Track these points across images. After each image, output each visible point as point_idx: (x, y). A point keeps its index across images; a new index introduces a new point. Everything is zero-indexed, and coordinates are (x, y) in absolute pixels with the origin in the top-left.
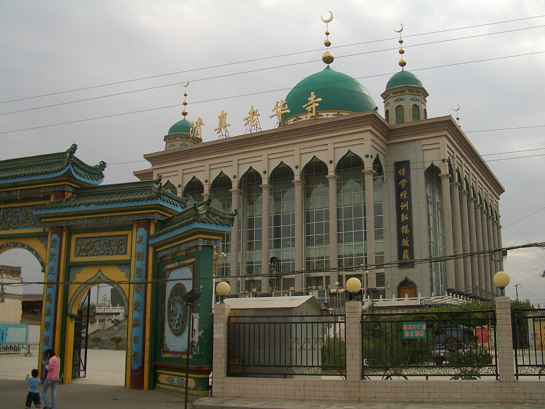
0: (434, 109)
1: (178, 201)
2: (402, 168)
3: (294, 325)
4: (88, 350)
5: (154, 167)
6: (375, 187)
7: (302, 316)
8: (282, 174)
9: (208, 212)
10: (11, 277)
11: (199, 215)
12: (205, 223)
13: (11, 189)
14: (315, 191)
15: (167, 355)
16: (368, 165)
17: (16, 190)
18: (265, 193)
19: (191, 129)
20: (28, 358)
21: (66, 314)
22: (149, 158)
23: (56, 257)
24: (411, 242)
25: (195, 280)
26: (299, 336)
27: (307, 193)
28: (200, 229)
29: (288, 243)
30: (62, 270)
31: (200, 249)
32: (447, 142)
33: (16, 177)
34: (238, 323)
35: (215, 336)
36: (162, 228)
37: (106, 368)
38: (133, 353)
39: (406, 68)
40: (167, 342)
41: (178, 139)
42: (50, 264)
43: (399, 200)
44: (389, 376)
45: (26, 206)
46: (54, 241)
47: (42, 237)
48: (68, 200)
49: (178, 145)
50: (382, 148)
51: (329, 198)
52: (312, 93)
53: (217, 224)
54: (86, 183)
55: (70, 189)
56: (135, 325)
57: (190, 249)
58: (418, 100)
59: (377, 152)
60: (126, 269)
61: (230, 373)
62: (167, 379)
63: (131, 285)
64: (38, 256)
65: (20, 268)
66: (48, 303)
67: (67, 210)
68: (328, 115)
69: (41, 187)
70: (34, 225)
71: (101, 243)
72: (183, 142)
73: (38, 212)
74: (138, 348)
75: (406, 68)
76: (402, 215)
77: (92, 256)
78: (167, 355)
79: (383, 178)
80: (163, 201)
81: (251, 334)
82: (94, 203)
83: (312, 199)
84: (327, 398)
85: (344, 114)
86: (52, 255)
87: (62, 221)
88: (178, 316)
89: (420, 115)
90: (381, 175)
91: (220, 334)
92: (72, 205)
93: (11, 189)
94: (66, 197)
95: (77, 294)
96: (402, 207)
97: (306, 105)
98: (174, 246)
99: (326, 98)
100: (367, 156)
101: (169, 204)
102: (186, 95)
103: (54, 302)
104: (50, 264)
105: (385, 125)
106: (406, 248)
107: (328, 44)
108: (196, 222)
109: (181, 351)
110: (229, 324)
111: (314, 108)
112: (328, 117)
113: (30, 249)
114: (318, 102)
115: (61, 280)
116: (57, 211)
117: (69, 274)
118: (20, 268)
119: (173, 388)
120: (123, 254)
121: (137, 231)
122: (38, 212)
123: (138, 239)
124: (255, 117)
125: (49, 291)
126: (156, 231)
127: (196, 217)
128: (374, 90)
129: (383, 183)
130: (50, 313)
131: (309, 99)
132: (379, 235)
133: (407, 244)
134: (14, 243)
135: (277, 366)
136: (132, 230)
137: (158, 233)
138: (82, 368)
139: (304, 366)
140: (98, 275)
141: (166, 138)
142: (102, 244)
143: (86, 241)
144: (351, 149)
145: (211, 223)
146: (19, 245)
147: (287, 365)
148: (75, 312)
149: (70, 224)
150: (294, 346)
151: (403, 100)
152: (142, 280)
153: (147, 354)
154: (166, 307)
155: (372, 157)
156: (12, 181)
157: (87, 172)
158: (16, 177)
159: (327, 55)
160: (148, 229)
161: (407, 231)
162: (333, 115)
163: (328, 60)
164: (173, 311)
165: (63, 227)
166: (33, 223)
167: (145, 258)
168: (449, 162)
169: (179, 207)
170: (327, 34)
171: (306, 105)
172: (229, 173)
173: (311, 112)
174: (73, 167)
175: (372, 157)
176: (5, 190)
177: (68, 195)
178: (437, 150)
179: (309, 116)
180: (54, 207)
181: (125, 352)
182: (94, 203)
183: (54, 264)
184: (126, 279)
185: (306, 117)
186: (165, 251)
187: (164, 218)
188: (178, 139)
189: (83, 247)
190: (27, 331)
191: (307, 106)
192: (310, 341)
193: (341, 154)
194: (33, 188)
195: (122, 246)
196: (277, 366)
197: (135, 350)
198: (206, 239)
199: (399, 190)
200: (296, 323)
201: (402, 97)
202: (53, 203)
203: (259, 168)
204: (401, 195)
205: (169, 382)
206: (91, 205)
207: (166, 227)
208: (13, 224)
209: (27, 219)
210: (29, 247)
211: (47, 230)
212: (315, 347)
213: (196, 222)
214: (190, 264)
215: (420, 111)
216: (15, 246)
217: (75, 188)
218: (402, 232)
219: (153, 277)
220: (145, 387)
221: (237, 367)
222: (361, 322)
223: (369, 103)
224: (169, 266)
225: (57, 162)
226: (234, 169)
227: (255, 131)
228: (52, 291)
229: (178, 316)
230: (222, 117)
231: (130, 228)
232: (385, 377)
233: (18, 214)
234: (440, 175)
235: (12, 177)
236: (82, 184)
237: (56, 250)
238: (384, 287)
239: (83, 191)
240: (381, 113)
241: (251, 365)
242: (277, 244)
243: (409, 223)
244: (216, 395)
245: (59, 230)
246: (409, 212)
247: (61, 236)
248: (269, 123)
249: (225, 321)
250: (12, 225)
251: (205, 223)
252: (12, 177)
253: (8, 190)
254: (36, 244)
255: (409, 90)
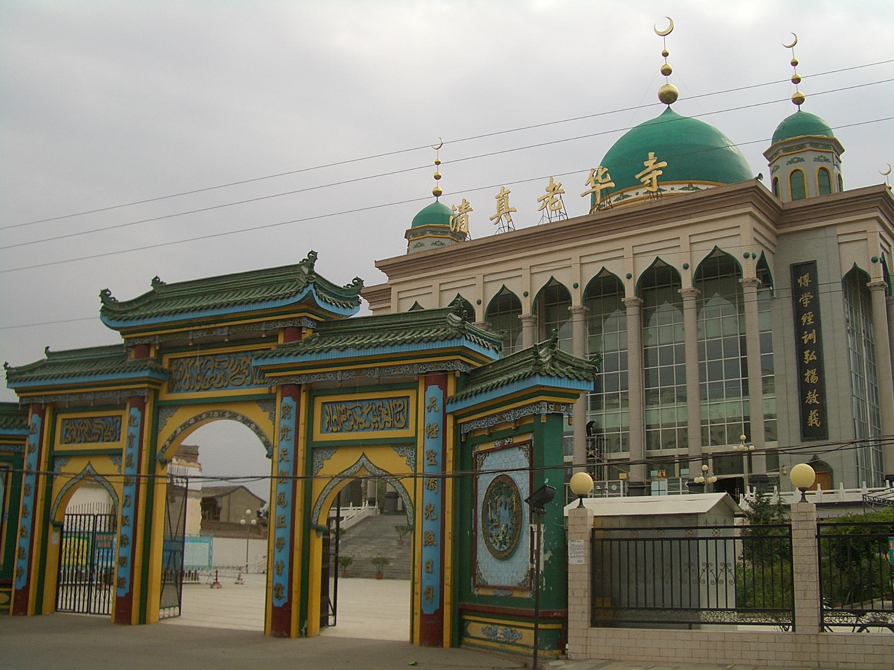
0: (855, 174)
1: (490, 341)
2: (804, 271)
3: (702, 543)
4: (339, 580)
5: (392, 282)
6: (761, 305)
7: (716, 527)
8: (604, 289)
9: (553, 359)
10: (184, 462)
11: (541, 365)
12: (551, 376)
13: (212, 326)
14: (655, 316)
15: (482, 592)
16: (749, 271)
17: (221, 327)
18: (577, 318)
19: (451, 218)
20: (215, 591)
21: (308, 526)
22: (385, 266)
23: (292, 434)
24: (822, 397)
25: (534, 470)
26: (712, 560)
27: (645, 318)
28: (544, 386)
29: (615, 401)
30: (301, 454)
31: (544, 420)
32: (879, 229)
33: (222, 306)
34: (608, 540)
35: (572, 561)
36: (466, 385)
37: (374, 610)
38: (424, 589)
39: (804, 108)
40: (482, 571)
41: (428, 234)
42: (281, 446)
43: (800, 328)
44: (863, 627)
45: (237, 353)
46: (286, 408)
47: (266, 401)
48: (308, 341)
49: (428, 245)
50: (767, 239)
51: (687, 327)
52: (651, 155)
53: (571, 379)
54: (333, 313)
55: (310, 324)
56: (427, 543)
57: (522, 419)
58: (827, 160)
59: (761, 248)
60: (409, 452)
61: (596, 622)
62: (483, 630)
64: (258, 432)
65: (197, 447)
66: (279, 508)
67: (307, 358)
68: (672, 189)
69: (262, 322)
70: (252, 383)
71: (364, 410)
72: (437, 240)
73: (260, 363)
74: (432, 581)
75: (804, 108)
76: (807, 353)
77: (350, 431)
78: (482, 592)
79: (772, 291)
80: (468, 342)
81: (639, 556)
82: (354, 346)
83: (651, 330)
84: (763, 663)
85: (703, 187)
86: (285, 430)
87: (300, 375)
88: (502, 529)
89: (832, 185)
90: (768, 286)
91: (579, 557)
92: (317, 350)
93: (212, 326)
94: (304, 337)
95: (325, 493)
96: (806, 338)
97: (641, 174)
98: (494, 415)
99: (667, 162)
100: (746, 256)
101: (477, 346)
103: (289, 507)
104: (281, 446)
105: (775, 204)
106: (813, 406)
107: (667, 72)
108: (538, 376)
109: (509, 585)
110: (593, 540)
111: (655, 178)
112: (673, 192)
113: (246, 421)
114: (660, 169)
115: (300, 473)
116: (292, 360)
117: (312, 461)
118: (197, 447)
119: (497, 645)
120: (402, 428)
121: (425, 391)
122: (260, 363)
123: (428, 404)
124: (557, 196)
125: (282, 488)
126: (457, 391)
127: (537, 368)
128: (750, 147)
129: (773, 299)
130: (284, 524)
131: (646, 164)
132: (768, 385)
133: (815, 401)
134: (218, 411)
135: (677, 609)
136: (417, 388)
137: (459, 394)
138: (331, 612)
139: (722, 610)
140: (361, 463)
141: (408, 234)
142: (366, 412)
143: (338, 407)
144: (721, 245)
145: (560, 377)
146: (227, 415)
147: (648, 606)
148: (323, 522)
149: (312, 380)
150: (703, 577)
151: (802, 160)
152: (436, 470)
153: (447, 590)
154: (480, 513)
155: (754, 258)
156: (216, 312)
157: (341, 298)
158: (222, 306)
159: (667, 89)
160: (444, 387)
161: (814, 379)
162: (682, 189)
163: (668, 97)
164: (492, 521)
165: (300, 386)
166: (249, 378)
167: (441, 434)
168: (884, 263)
169: (492, 351)
170: (665, 55)
171: (641, 174)
172: (517, 288)
173: (650, 185)
174: (315, 288)
175: (754, 258)
176: (204, 327)
177: (307, 334)
178: (863, 243)
179: (641, 192)
180: (286, 354)
181: (408, 583)
182: (354, 346)
183: (288, 445)
184: (409, 470)
185: (637, 194)
186: (472, 423)
187: (468, 370)
188: (428, 234)
189: (335, 417)
190: (211, 548)
191: (643, 176)
192: (713, 567)
193: (702, 253)
194: (249, 324)
195: (399, 416)
196: (677, 609)
197: (427, 583)
198: (551, 403)
199: (799, 311)
200: (707, 539)
201: (800, 156)
202: (283, 346)
203: (566, 279)
204: (804, 319)
205: (488, 635)
206: (348, 349)
207: (477, 383)
208: (217, 381)
209: (239, 373)
210: (243, 418)
211: (273, 390)
212: (722, 577)
213: (538, 376)
214: (524, 443)
215: (832, 179)
216: (222, 416)
217: (317, 321)
218: (807, 380)
219: (455, 468)
220: (445, 645)
221: (606, 613)
222: (818, 537)
223: (740, 166)
224: (482, 448)
225: (287, 281)
226: (525, 282)
227: (557, 219)
228: (286, 488)
229: (502, 529)
230: (503, 198)
231: (413, 385)
232: (857, 628)
233: (225, 365)
234: (868, 284)
235: (215, 307)
236: (328, 315)
237: (290, 423)
238: (778, 473)
239: (331, 327)
240: (767, 183)
241: (632, 609)
242: (596, 404)
243: (818, 365)
244: (573, 657)
245: (294, 390)
246: (817, 347)
247: (297, 399)
248: (578, 206)
249: (587, 536)
250: (215, 383)
251: (551, 376)
252: (215, 307)
253: (208, 327)
254: (257, 414)
255: (812, 144)
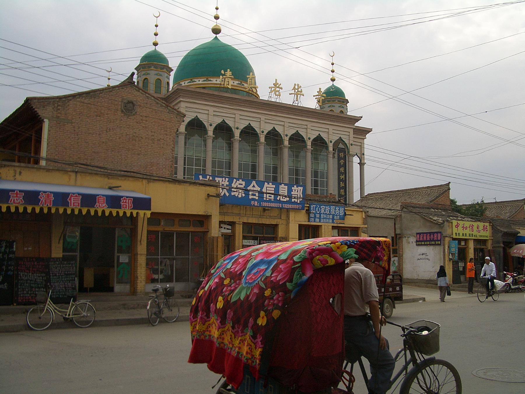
39: (158, 48)
58: (161, 75)
63: (391, 223)
102: (156, 26)
201: (161, 73)
